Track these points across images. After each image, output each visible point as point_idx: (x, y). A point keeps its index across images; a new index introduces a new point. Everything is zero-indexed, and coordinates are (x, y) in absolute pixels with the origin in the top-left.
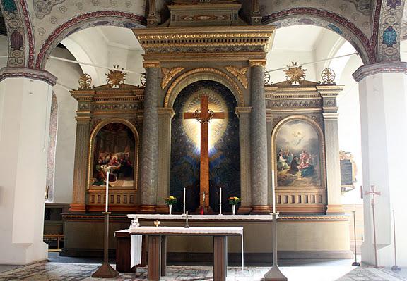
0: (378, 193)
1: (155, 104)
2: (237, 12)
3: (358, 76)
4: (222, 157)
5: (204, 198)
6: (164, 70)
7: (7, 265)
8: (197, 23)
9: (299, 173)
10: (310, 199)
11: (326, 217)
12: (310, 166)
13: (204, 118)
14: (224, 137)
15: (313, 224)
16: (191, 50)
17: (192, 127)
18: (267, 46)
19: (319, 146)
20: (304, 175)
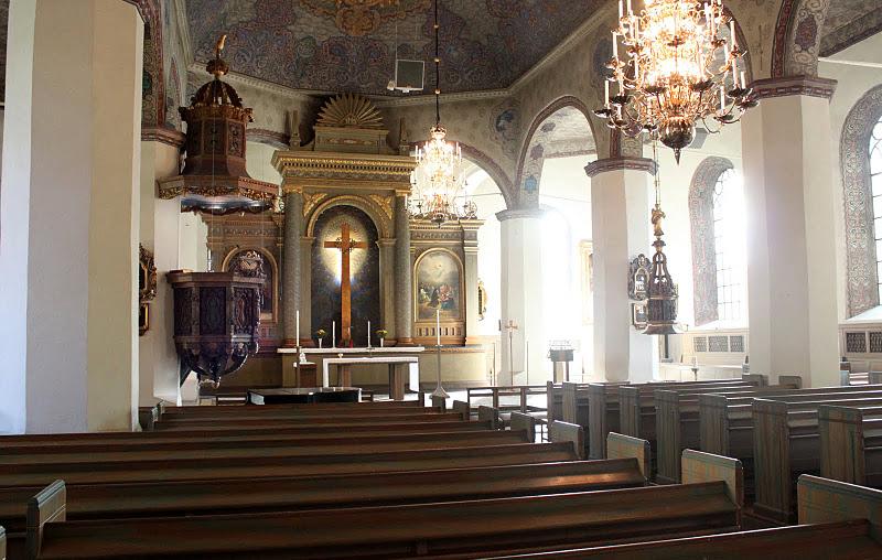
0: (516, 328)
1: (298, 233)
2: (384, 139)
3: (500, 216)
4: (362, 288)
5: (347, 332)
6: (307, 196)
7: (555, 372)
8: (343, 148)
9: (440, 306)
10: (450, 331)
11: (463, 349)
12: (455, 297)
13: (346, 248)
14: (364, 267)
15: (462, 355)
16: (335, 176)
17: (332, 258)
18: (413, 176)
19: (459, 279)
20: (445, 308)
